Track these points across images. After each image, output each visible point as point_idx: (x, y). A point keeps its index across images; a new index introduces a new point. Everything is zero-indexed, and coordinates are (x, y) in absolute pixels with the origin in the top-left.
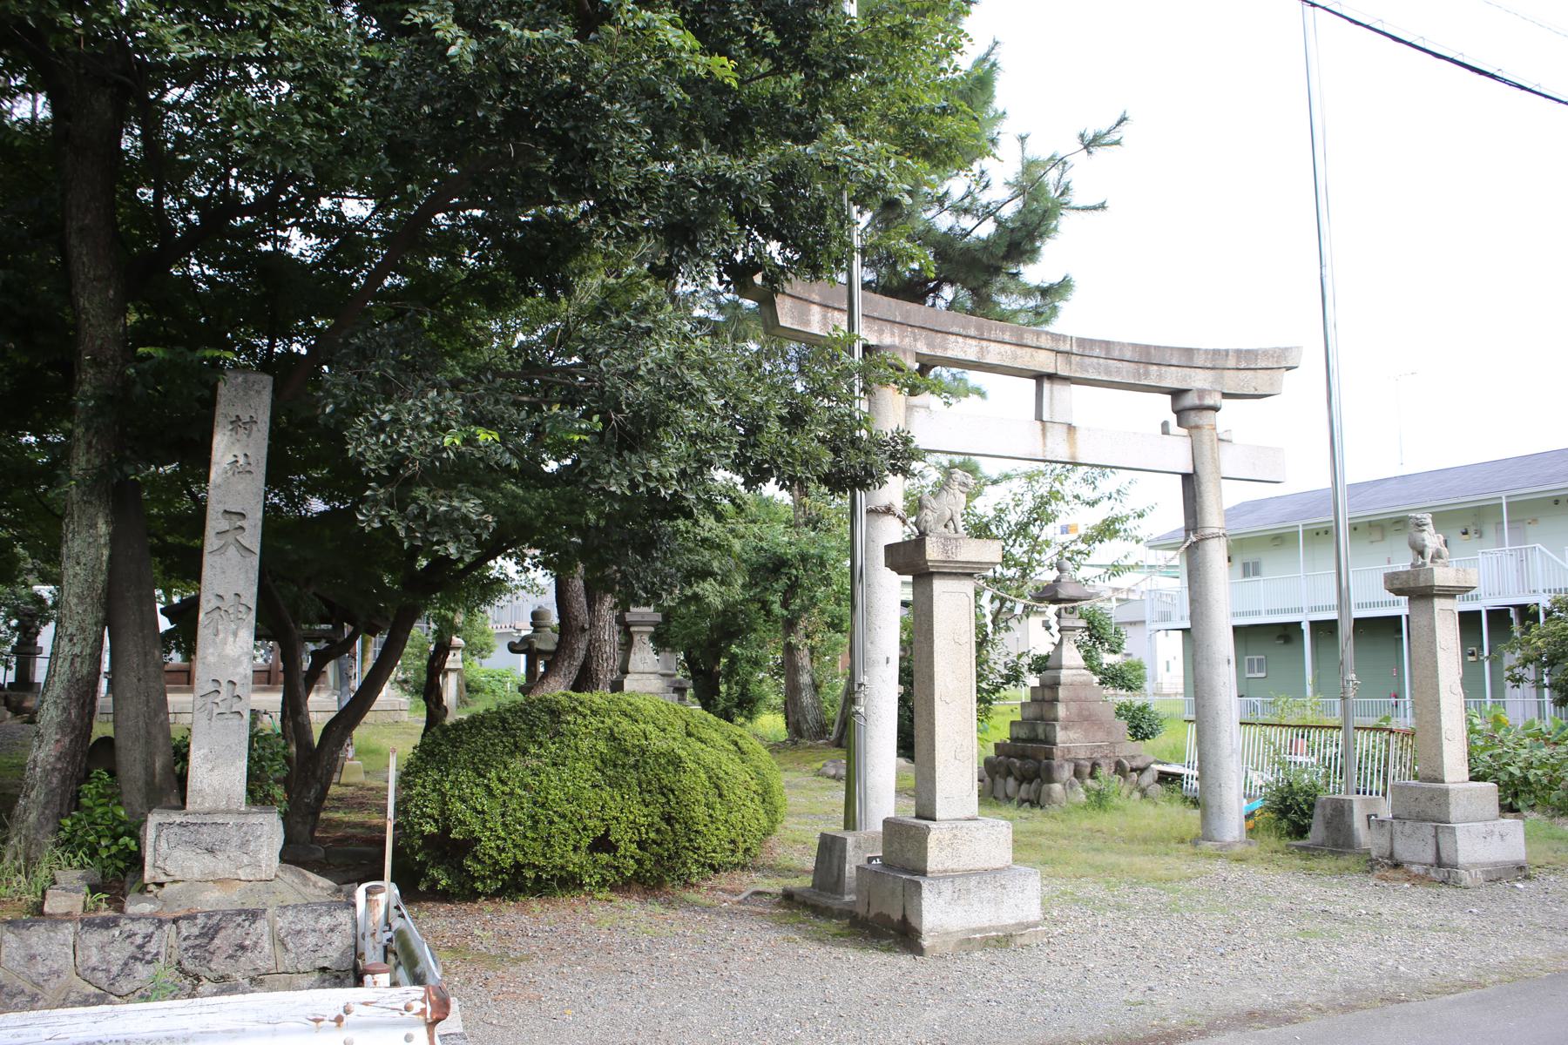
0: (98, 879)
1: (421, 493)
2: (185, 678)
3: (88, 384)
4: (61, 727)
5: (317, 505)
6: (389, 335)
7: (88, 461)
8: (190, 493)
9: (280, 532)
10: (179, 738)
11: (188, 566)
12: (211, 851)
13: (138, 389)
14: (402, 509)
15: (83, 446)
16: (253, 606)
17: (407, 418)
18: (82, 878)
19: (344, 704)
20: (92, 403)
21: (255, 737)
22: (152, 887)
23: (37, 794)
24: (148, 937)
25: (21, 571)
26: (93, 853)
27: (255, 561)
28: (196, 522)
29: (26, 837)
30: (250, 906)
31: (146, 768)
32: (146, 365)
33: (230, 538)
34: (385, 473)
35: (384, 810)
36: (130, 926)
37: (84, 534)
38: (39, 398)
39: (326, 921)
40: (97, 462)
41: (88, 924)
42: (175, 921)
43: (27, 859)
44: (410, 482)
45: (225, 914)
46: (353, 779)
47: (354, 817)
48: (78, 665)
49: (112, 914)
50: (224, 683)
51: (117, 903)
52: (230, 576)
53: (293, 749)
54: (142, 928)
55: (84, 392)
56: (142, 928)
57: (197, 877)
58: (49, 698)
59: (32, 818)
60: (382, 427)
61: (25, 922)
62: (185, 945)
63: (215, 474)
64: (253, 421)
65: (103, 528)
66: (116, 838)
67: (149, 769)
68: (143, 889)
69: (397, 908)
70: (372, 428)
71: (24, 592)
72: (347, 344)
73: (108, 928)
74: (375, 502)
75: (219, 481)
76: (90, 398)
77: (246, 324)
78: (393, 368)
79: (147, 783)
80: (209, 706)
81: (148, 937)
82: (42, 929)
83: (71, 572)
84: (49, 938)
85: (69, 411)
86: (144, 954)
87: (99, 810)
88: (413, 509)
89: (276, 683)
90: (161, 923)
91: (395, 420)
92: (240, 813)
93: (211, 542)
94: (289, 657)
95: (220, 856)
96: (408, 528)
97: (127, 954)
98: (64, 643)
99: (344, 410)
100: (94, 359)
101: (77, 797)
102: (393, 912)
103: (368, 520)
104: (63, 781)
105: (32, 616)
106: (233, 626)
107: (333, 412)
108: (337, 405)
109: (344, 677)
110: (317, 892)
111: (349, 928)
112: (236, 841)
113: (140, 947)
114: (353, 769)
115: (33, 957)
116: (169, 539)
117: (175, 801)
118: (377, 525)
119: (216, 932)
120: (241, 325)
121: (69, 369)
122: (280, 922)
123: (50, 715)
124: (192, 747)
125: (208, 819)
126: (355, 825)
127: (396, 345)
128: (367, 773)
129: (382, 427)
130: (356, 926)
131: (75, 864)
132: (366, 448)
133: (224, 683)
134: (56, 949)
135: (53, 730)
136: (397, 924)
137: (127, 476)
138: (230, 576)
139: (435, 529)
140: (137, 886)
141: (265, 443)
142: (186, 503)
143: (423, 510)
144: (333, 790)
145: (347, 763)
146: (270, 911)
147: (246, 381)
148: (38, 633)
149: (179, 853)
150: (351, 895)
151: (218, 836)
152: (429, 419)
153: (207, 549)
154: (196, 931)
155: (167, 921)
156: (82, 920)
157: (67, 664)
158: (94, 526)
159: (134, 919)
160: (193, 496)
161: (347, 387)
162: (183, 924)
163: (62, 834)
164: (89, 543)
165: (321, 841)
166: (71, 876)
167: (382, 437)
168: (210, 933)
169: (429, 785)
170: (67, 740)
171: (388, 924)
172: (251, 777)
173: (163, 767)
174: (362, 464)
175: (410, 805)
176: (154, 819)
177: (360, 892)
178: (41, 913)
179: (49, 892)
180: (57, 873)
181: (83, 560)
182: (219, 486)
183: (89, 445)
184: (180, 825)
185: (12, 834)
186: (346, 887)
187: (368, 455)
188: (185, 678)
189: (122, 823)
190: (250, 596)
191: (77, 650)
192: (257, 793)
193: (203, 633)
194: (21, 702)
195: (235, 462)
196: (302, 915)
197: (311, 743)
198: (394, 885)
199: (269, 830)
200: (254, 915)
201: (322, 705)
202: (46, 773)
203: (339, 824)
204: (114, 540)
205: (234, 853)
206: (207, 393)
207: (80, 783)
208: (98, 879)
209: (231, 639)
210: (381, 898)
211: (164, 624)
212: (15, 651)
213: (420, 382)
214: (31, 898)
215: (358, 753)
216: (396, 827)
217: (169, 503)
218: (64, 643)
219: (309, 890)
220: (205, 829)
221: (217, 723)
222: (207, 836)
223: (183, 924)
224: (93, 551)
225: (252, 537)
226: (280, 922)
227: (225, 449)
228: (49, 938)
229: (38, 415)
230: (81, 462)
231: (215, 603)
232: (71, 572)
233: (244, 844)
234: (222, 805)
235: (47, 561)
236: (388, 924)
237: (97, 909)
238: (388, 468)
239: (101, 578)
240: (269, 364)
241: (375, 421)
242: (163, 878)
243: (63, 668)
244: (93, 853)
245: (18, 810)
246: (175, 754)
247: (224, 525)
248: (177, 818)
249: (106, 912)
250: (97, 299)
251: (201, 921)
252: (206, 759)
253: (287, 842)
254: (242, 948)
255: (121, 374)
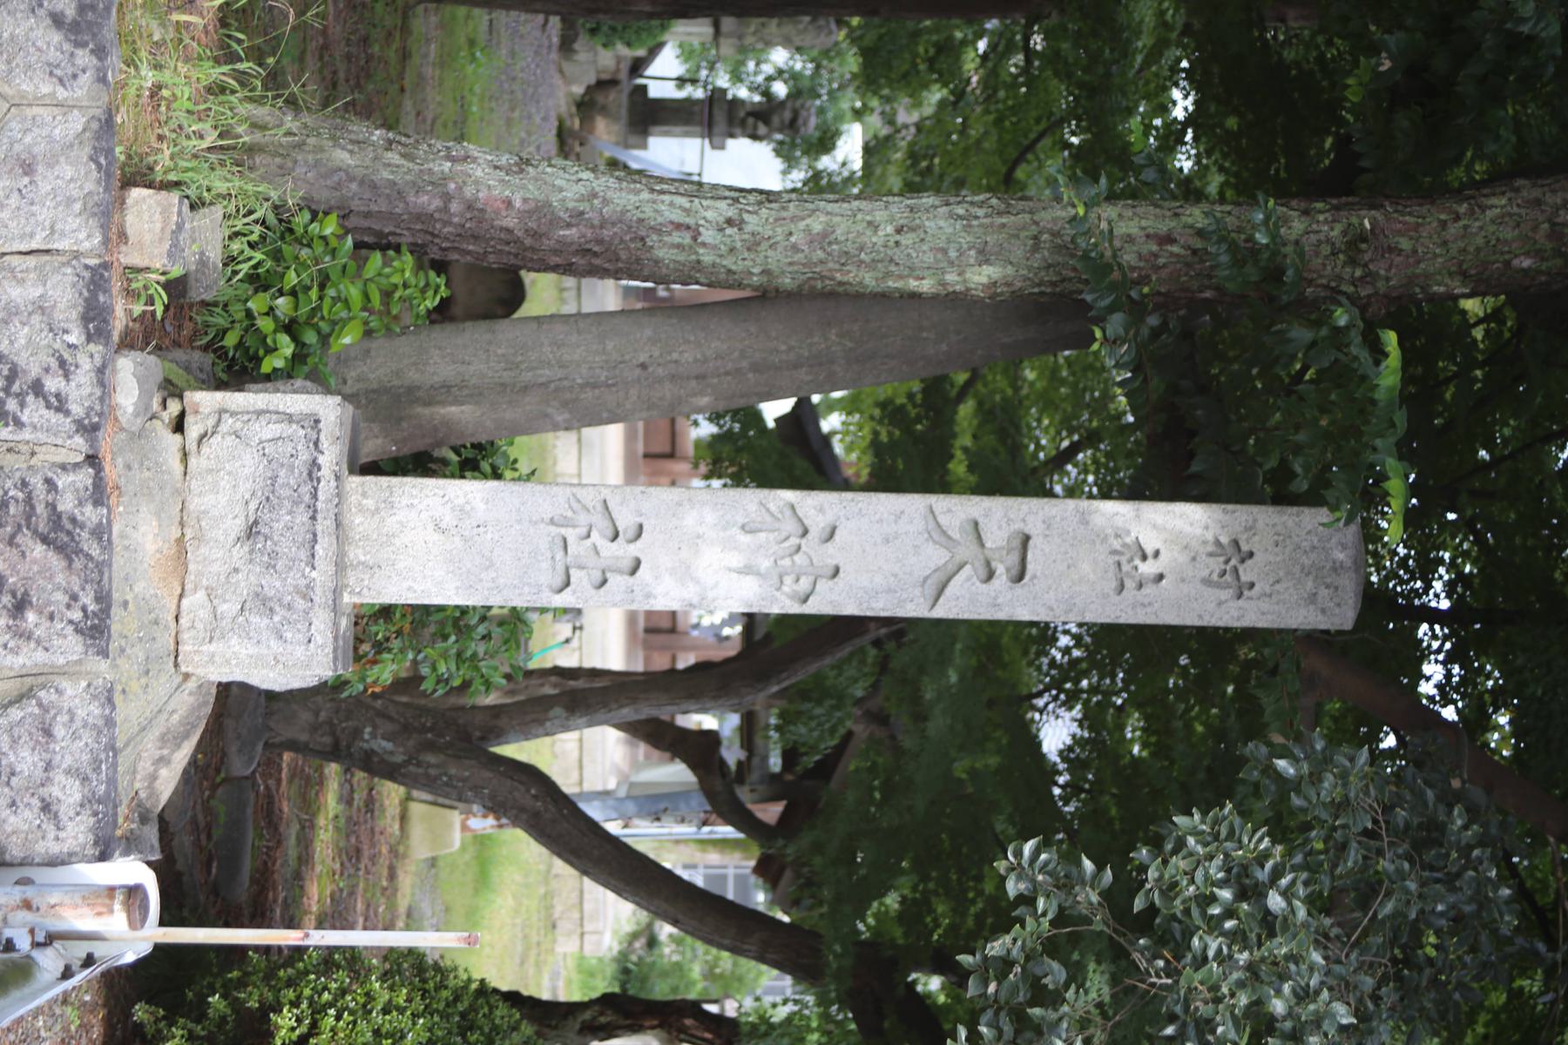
0: (197, 293)
1: (1098, 985)
2: (656, 458)
3: (1307, 230)
4: (540, 209)
5: (1056, 733)
6: (1483, 902)
7: (1130, 239)
8: (1068, 455)
9: (999, 658)
10: (513, 452)
11: (911, 459)
12: (252, 531)
13: (1301, 334)
14: (1052, 947)
15: (1163, 227)
16: (811, 608)
17: (1280, 947)
18: (203, 262)
19: (593, 811)
20: (1262, 238)
21: (514, 623)
22: (174, 407)
23: (393, 166)
24: (59, 404)
25: (888, 100)
26: (258, 281)
27: (914, 607)
28: (1008, 473)
29: (300, 146)
30: (119, 622)
31: (447, 387)
32: (1357, 349)
33: (967, 550)
34: (1138, 904)
35: (335, 918)
36: (86, 364)
37: (965, 240)
38: (1270, 126)
39: (68, 793)
40: (1128, 258)
41: (97, 280)
42: (92, 459)
43: (251, 149)
44: (1117, 956)
45: (102, 566)
46: (417, 831)
47: (325, 839)
48: (676, 238)
49: (119, 322)
50: (634, 550)
51: (144, 336)
52: (880, 554)
53: (491, 699)
54: (80, 390)
55: (1286, 221)
56: (80, 390)
57: (194, 504)
58: (604, 183)
59: (342, 157)
60: (1250, 891)
61: (109, 152)
62: (37, 482)
63: (1115, 512)
64: (1242, 590)
65: (981, 277)
66: (290, 328)
67: (446, 392)
68: (171, 389)
69: (89, 961)
70: (1245, 869)
71: (845, 105)
72: (1449, 799)
73: (86, 319)
74: (1066, 884)
75: (1098, 521)
76: (1274, 236)
77: (1485, 556)
78: (1397, 914)
79: (411, 390)
80: (583, 519)
81: (59, 404)
82: (90, 186)
83: (880, 216)
84: (70, 201)
85: (1244, 189)
86: (21, 397)
87: (354, 293)
88: (1055, 973)
89: (648, 647)
90: (89, 429)
91: (1269, 924)
92: (337, 592)
93: (955, 510)
94: (708, 680)
95: (240, 552)
96: (1006, 963)
97: (21, 360)
98: (724, 209)
99: (1283, 797)
100: (1363, 237)
101: (386, 245)
102: (80, 950)
103: (1024, 865)
104: (421, 217)
105: (793, 125)
106: (765, 564)
107: (1278, 776)
108: (1296, 785)
109: (656, 804)
110: (145, 766)
111: (52, 847)
112: (273, 585)
113: (37, 388)
114: (440, 829)
115: (28, 169)
116: (966, 410)
117: (372, 449)
118: (1013, 887)
119: (60, 549)
120: (1480, 540)
121: (1339, 184)
122: (73, 691)
123: (568, 187)
124: (493, 484)
125: (325, 524)
126: (306, 843)
127: (1458, 919)
128: (433, 862)
129: (1250, 891)
130: (54, 862)
131: (236, 246)
132: (1196, 857)
133: (634, 550)
134: (44, 214)
135: (533, 191)
136: (49, 962)
137: (1100, 321)
138: (880, 554)
139: (1008, 1029)
140: (178, 376)
141: (1190, 620)
142: (1043, 439)
143: (1053, 999)
144: (392, 793)
145: (456, 817)
146: (103, 665)
147: (1337, 568)
148: (755, 137)
149: (249, 464)
150: (131, 845)
151: (287, 547)
152: (1278, 1006)
153: (939, 502)
154: (66, 504)
155: (92, 442)
156: (106, 266)
157: (677, 216)
158: (984, 257)
159: (102, 374)
160: (1061, 459)
161: (1341, 806)
162: (85, 477)
163: (302, 219)
164: (952, 250)
165: (270, 765)
166: (208, 237)
167: (1226, 894)
168: (59, 535)
169: (387, 1022)
170: (510, 222)
171: (51, 939)
172: (422, 614)
173: (447, 423)
174: (1156, 844)
175: (343, 977)
176: (329, 409)
177: (135, 871)
178: (128, 182)
179: (174, 197)
180: (218, 211)
181: (907, 239)
182: (1084, 521)
183: (1168, 239)
184: (314, 465)
185: (307, 118)
186: (152, 833)
187: (1179, 863)
188: (656, 458)
189: (324, 339)
190: (830, 601)
191: (708, 235)
192: (378, 627)
193: (752, 500)
194: (604, 111)
195: (1136, 555)
196: (87, 737)
197: (500, 736)
198: (145, 949)
199: (293, 656)
200: (95, 631)
201: (590, 758)
202: (441, 181)
203: (309, 806)
204: (953, 300)
205: (245, 583)
206: (1302, 485)
207: (417, 250)
208: (197, 293)
209: (736, 560)
210: (115, 922)
211: (774, 410)
212: (717, 95)
213: (1368, 982)
214: (163, 159)
215: (481, 841)
216: (298, 951)
217: (1048, 403)
218: (724, 209)
219: (150, 747)
220: (302, 517)
221: (544, 537)
222: (286, 523)
223: (85, 477)
224: (929, 258)
225: (968, 600)
226: (73, 691)
227: (1174, 531)
228: (70, 201)
229: (1232, 123)
230: (1129, 227)
231: (817, 523)
232: (880, 216)
233: (263, 602)
234: (355, 554)
235: (913, 156)
236: (51, 939)
237: (131, 294)
238: (1152, 910)
239: (869, 280)
240: (1385, 620)
241: (1262, 875)
242: (193, 429)
243: (670, 209)
244: (258, 281)
245: (359, 128)
246: (478, 447)
247: (997, 536)
248: (331, 457)
249: (122, 313)
250: (1508, 233)
251: (90, 514)
252: (463, 512)
253: (271, 696)
254: (20, 606)
255: (1334, 295)
